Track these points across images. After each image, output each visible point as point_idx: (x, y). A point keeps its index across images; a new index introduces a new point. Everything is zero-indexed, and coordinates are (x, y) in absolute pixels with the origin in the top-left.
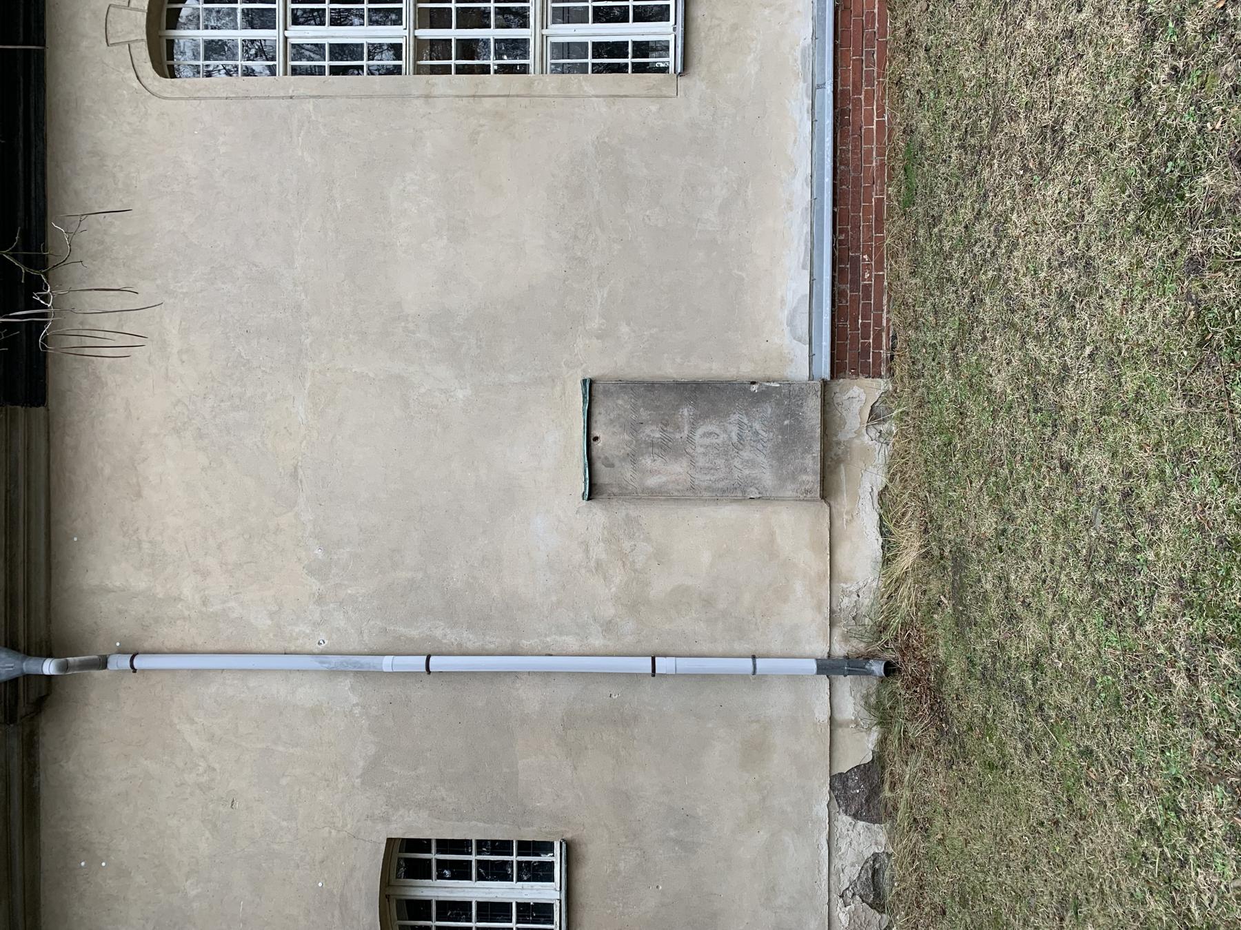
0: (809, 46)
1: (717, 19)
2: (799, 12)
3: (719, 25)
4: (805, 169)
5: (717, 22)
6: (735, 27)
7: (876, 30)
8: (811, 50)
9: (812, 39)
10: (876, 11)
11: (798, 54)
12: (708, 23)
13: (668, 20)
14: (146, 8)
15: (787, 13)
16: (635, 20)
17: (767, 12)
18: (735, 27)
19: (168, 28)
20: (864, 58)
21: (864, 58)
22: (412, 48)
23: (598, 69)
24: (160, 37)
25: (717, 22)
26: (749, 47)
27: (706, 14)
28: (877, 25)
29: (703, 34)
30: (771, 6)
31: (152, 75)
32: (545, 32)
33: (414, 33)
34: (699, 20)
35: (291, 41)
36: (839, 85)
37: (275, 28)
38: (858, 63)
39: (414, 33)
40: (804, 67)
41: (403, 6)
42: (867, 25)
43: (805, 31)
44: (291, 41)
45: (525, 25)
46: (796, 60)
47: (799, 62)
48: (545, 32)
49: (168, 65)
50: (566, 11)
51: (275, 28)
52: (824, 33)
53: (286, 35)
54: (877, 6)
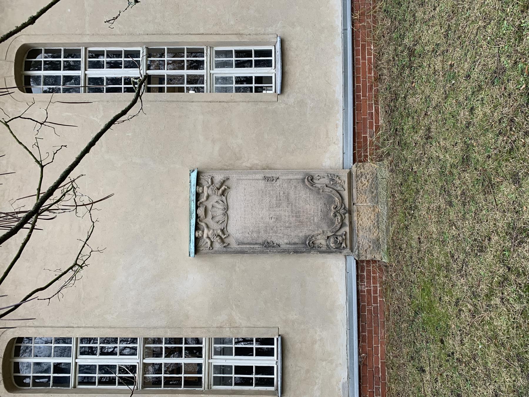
0: (346, 382)
1: (299, 367)
2: (340, 364)
3: (300, 370)
4: (340, 29)
5: (299, 368)
6: (308, 371)
7: (380, 376)
8: (347, 384)
9: (347, 379)
10: (380, 366)
11: (341, 386)
12: (294, 369)
13: (273, 356)
14: (3, 356)
15: (334, 364)
16: (257, 355)
17: (324, 363)
18: (308, 371)
19: (25, 70)
20: (374, 390)
21: (374, 390)
22: (141, 370)
23: (238, 90)
24: (10, 362)
25: (299, 368)
26: (315, 382)
27: (293, 364)
28: (380, 374)
29: (291, 375)
30: (326, 360)
31: (4, 391)
32: (212, 72)
33: (143, 361)
34: (289, 367)
35: (78, 364)
36: (355, 84)
37: (80, 70)
38: (371, 393)
39: (143, 361)
40: (344, 393)
41: (138, 345)
42: (376, 373)
43: (344, 375)
44: (78, 364)
45: (200, 356)
46: (339, 390)
47: (341, 390)
48: (212, 72)
49: (14, 376)
50: (222, 378)
51: (80, 70)
52: (354, 376)
53: (86, 73)
54: (380, 364)
